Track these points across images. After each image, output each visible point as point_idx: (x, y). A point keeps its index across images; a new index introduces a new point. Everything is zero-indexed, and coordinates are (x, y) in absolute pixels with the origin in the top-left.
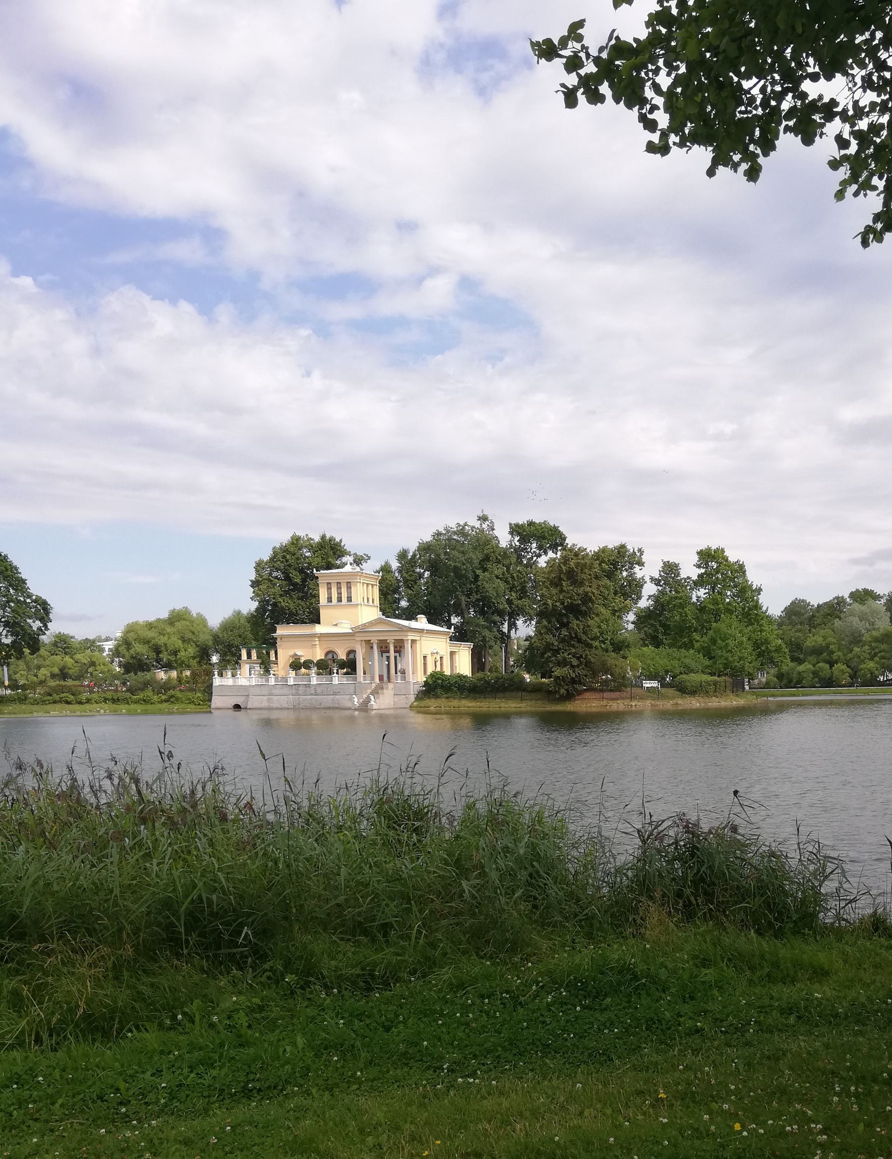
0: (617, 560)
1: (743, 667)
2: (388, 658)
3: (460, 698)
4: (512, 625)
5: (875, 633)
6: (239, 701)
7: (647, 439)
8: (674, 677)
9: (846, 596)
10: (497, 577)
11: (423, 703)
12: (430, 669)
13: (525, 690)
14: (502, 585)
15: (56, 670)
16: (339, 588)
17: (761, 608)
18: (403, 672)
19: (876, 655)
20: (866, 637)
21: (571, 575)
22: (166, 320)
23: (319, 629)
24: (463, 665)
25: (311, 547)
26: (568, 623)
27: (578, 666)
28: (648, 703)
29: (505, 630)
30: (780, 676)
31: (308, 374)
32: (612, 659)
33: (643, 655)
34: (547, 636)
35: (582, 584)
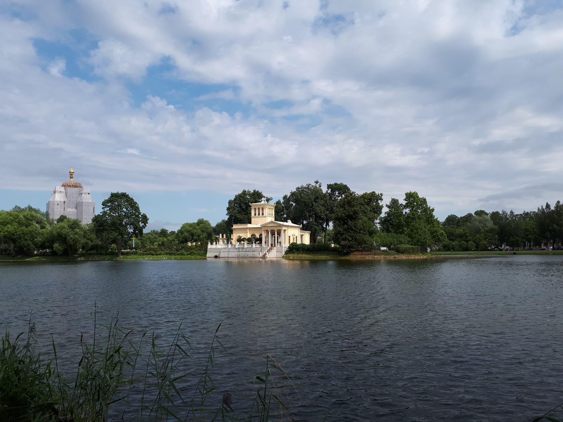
0: (372, 199)
4: (327, 224)
5: (486, 228)
6: (217, 254)
7: (393, 155)
9: (473, 213)
12: (292, 241)
13: (329, 250)
15: (160, 243)
16: (259, 210)
18: (280, 243)
19: (487, 238)
20: (482, 230)
21: (349, 203)
22: (217, 119)
23: (249, 226)
24: (307, 240)
25: (249, 195)
29: (325, 226)
30: (445, 246)
31: (266, 136)
32: (367, 238)
33: (381, 236)
35: (353, 206)
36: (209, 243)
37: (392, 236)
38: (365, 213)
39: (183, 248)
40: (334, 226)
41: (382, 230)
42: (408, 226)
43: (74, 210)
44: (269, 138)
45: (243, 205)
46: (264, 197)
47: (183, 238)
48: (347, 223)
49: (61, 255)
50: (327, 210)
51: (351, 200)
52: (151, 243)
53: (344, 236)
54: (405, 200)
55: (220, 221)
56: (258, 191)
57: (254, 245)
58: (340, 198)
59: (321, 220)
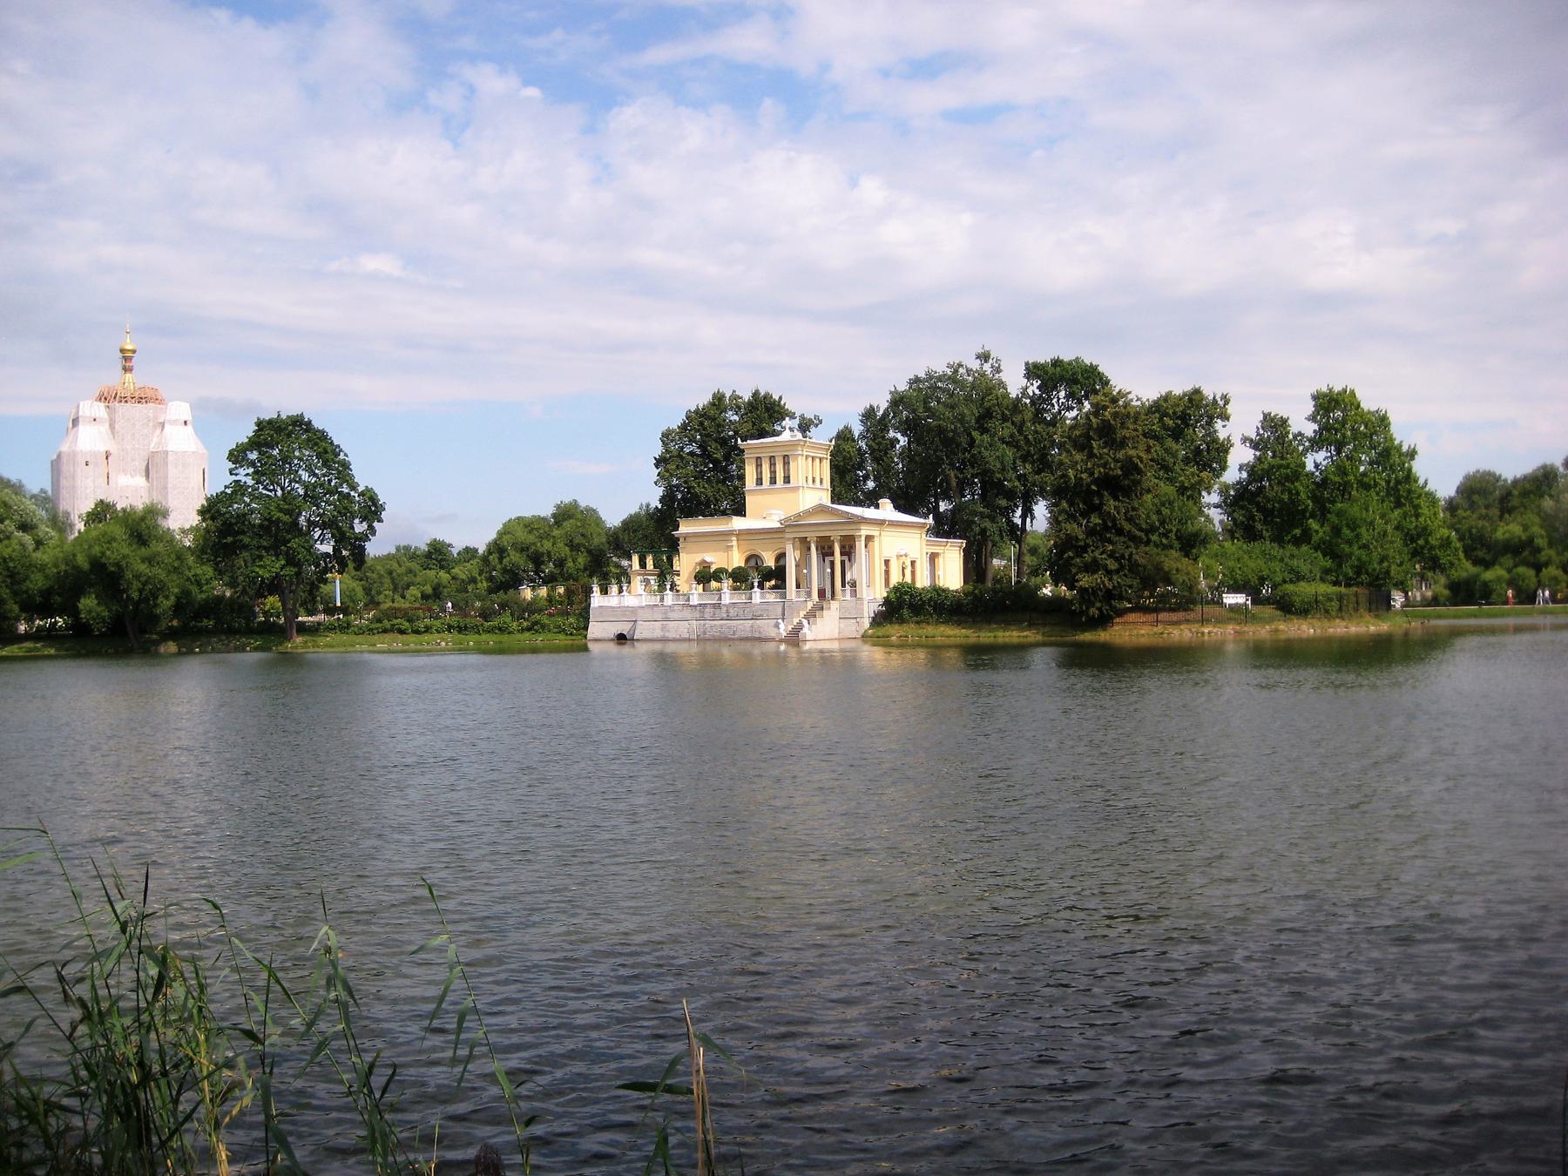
0: (1186, 420)
1: (1388, 572)
2: (832, 563)
3: (938, 623)
4: (1028, 512)
6: (624, 628)
8: (1274, 587)
10: (1003, 440)
11: (881, 631)
12: (895, 579)
14: (1010, 453)
15: (428, 589)
17: (1416, 481)
18: (854, 585)
23: (737, 523)
24: (951, 573)
26: (1101, 504)
27: (1117, 571)
28: (1230, 629)
29: (1018, 521)
32: (1172, 560)
33: (1224, 555)
34: (1068, 526)
35: (1123, 444)
36: (596, 588)
37: (1263, 553)
38: (1166, 468)
39: (503, 606)
40: (1054, 521)
41: (1230, 533)
42: (1322, 512)
43: (141, 481)
44: (872, 191)
45: (712, 446)
46: (792, 416)
47: (505, 571)
48: (1097, 509)
49: (103, 635)
50: (1024, 459)
51: (1111, 422)
52: (395, 590)
53: (1087, 557)
54: (1312, 418)
55: (633, 509)
56: (767, 396)
57: (757, 594)
58: (1074, 413)
59: (1001, 496)
